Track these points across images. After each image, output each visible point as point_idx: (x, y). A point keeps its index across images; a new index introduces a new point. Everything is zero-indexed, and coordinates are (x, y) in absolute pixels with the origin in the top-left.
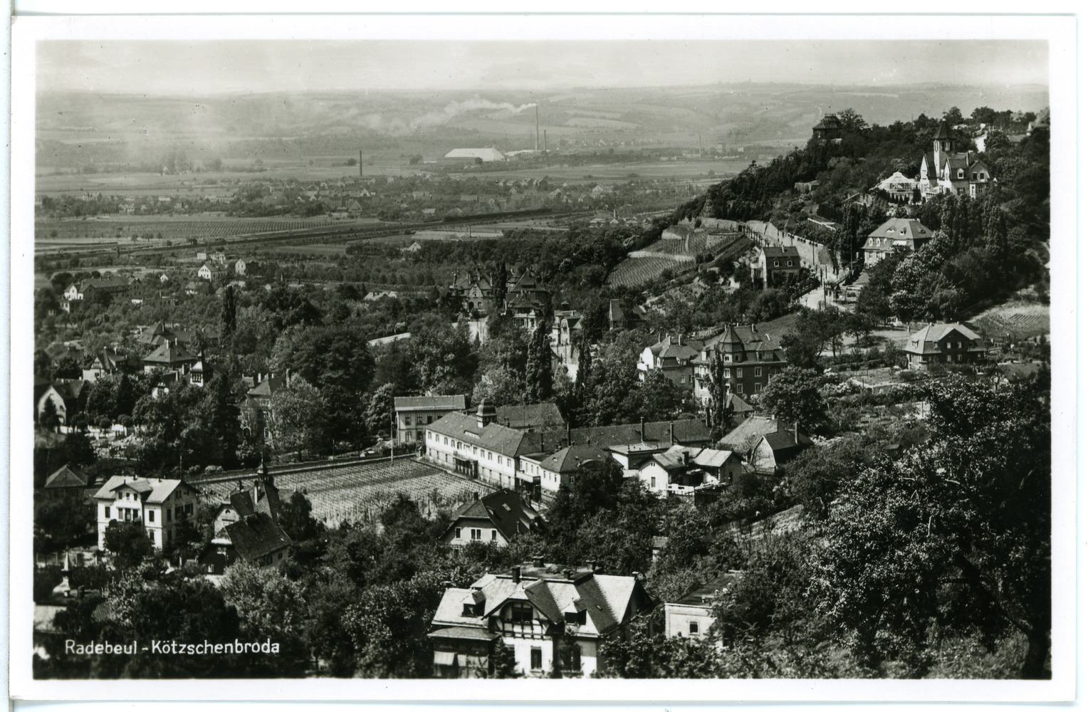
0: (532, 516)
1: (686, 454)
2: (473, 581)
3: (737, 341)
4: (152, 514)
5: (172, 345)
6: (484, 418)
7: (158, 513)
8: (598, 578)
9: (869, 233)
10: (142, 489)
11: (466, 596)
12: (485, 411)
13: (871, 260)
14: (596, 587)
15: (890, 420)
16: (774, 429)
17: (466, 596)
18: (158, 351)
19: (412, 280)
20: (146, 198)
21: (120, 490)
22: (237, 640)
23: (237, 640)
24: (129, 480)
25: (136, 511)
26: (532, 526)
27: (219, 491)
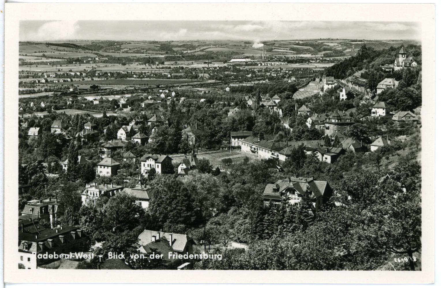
0: (279, 167)
1: (328, 149)
2: (275, 182)
3: (338, 115)
4: (158, 166)
5: (156, 116)
6: (260, 138)
7: (160, 165)
8: (316, 182)
9: (379, 82)
10: (156, 158)
11: (274, 186)
12: (260, 136)
13: (379, 92)
14: (314, 184)
15: (59, 259)
16: (354, 142)
17: (274, 186)
18: (153, 118)
19: (230, 99)
20: (62, 113)
21: (148, 158)
22: (55, 253)
23: (55, 253)
24: (150, 155)
25: (153, 165)
26: (279, 171)
27: (176, 159)
